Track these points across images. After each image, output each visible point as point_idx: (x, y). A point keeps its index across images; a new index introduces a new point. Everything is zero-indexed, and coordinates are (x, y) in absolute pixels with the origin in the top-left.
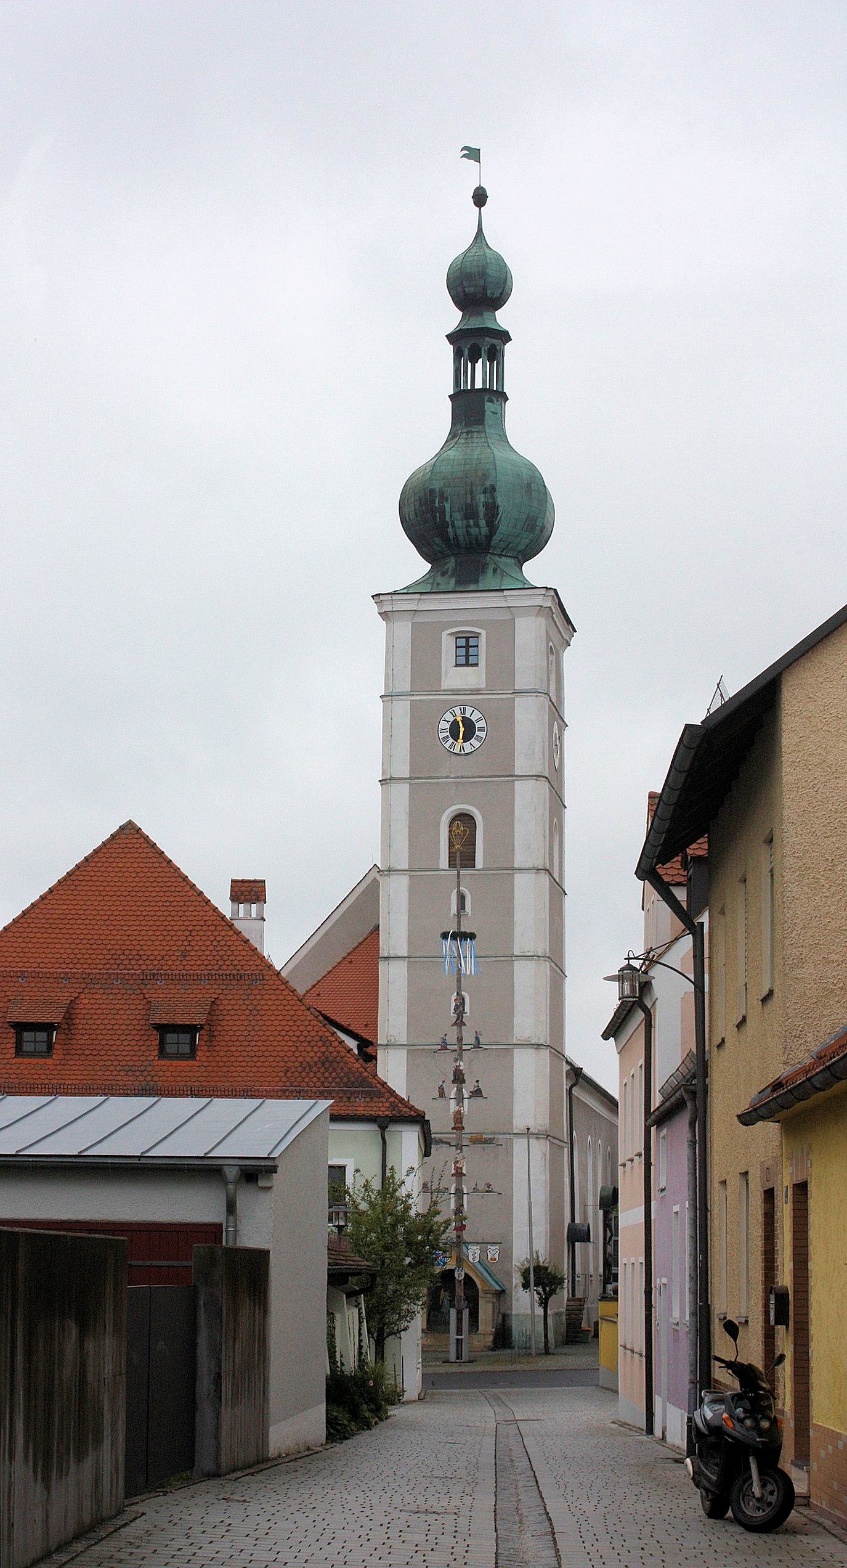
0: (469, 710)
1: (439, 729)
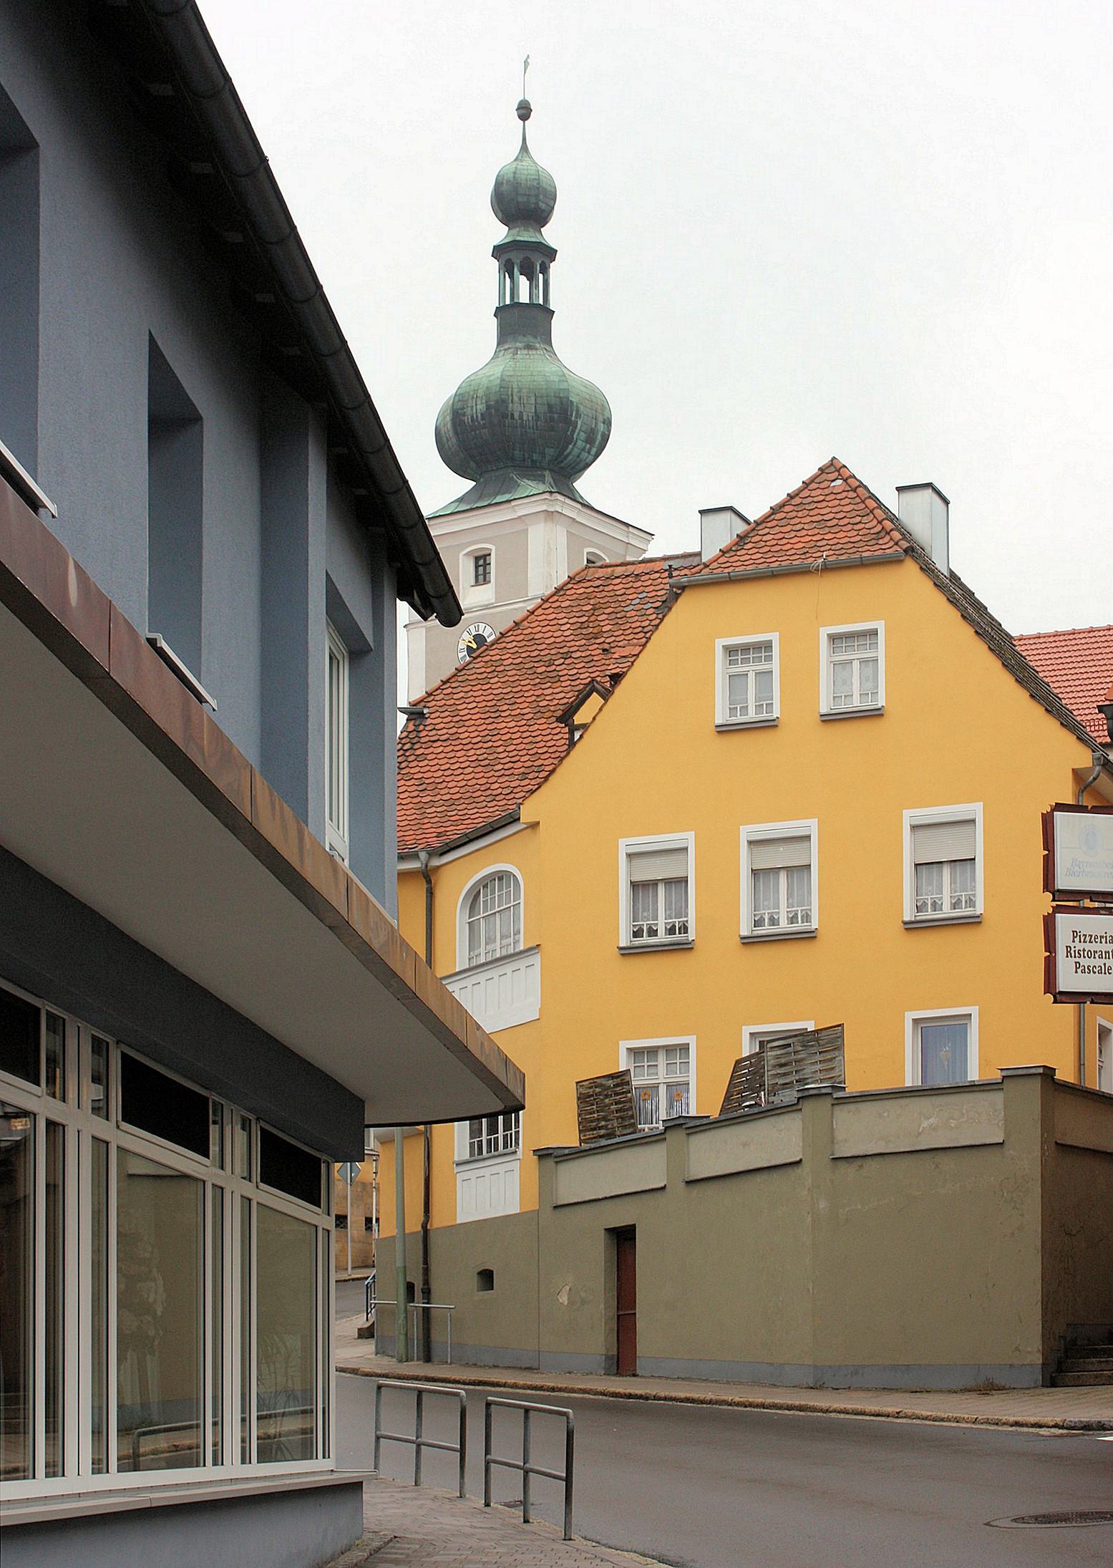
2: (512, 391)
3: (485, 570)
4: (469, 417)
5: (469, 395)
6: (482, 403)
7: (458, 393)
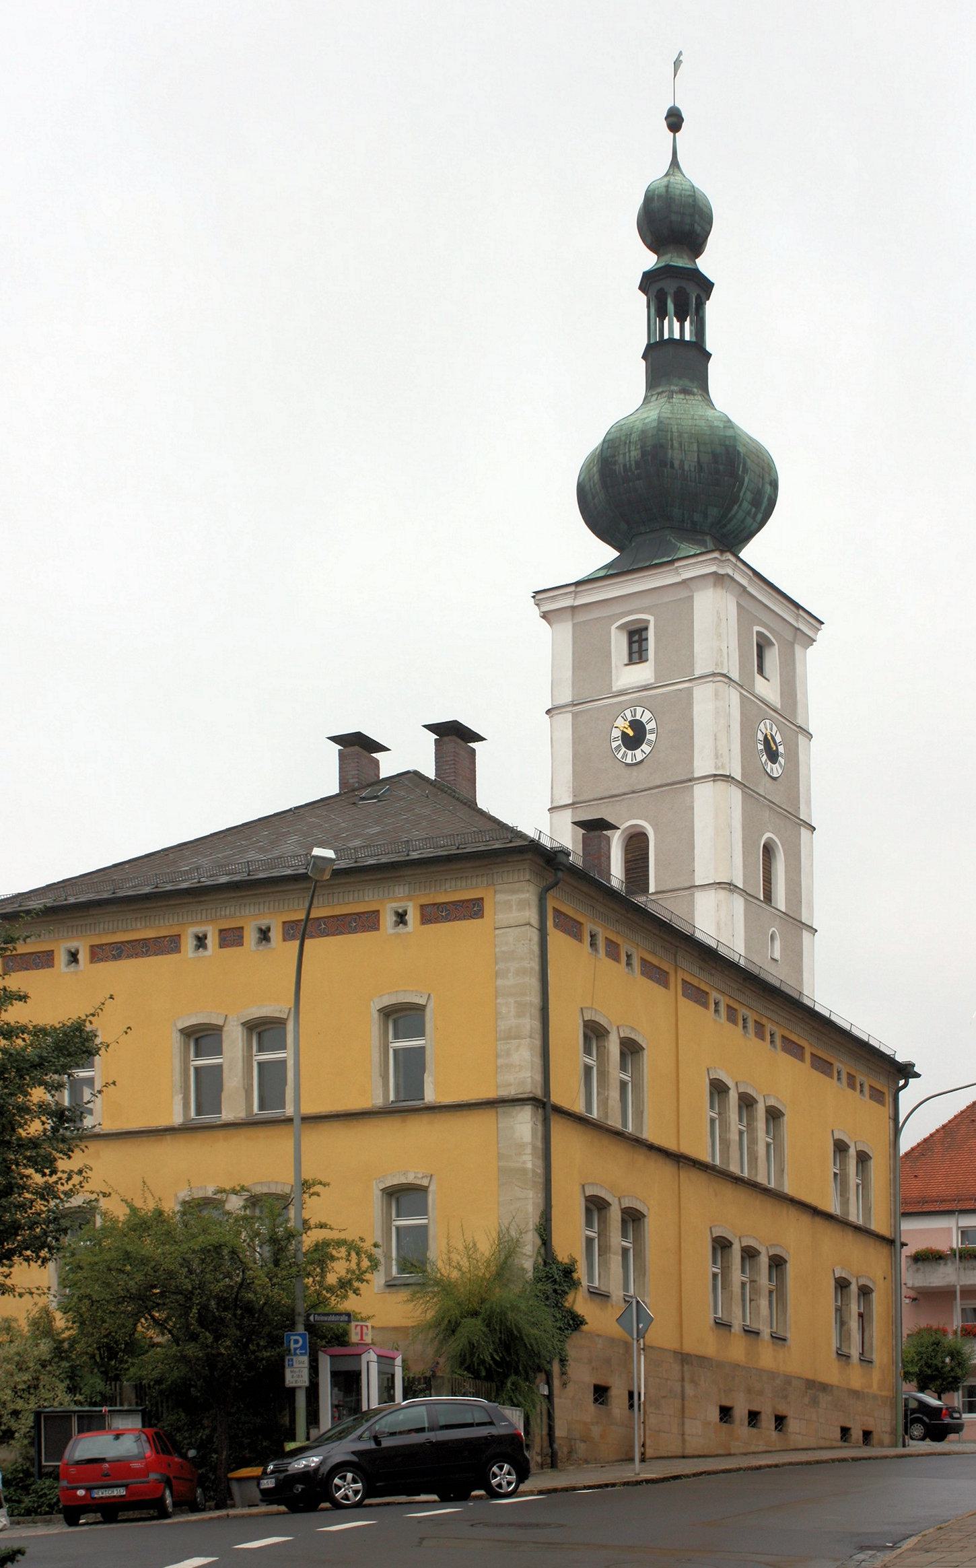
0: (639, 710)
2: (672, 435)
3: (640, 646)
4: (622, 466)
5: (620, 440)
6: (635, 450)
7: (607, 439)
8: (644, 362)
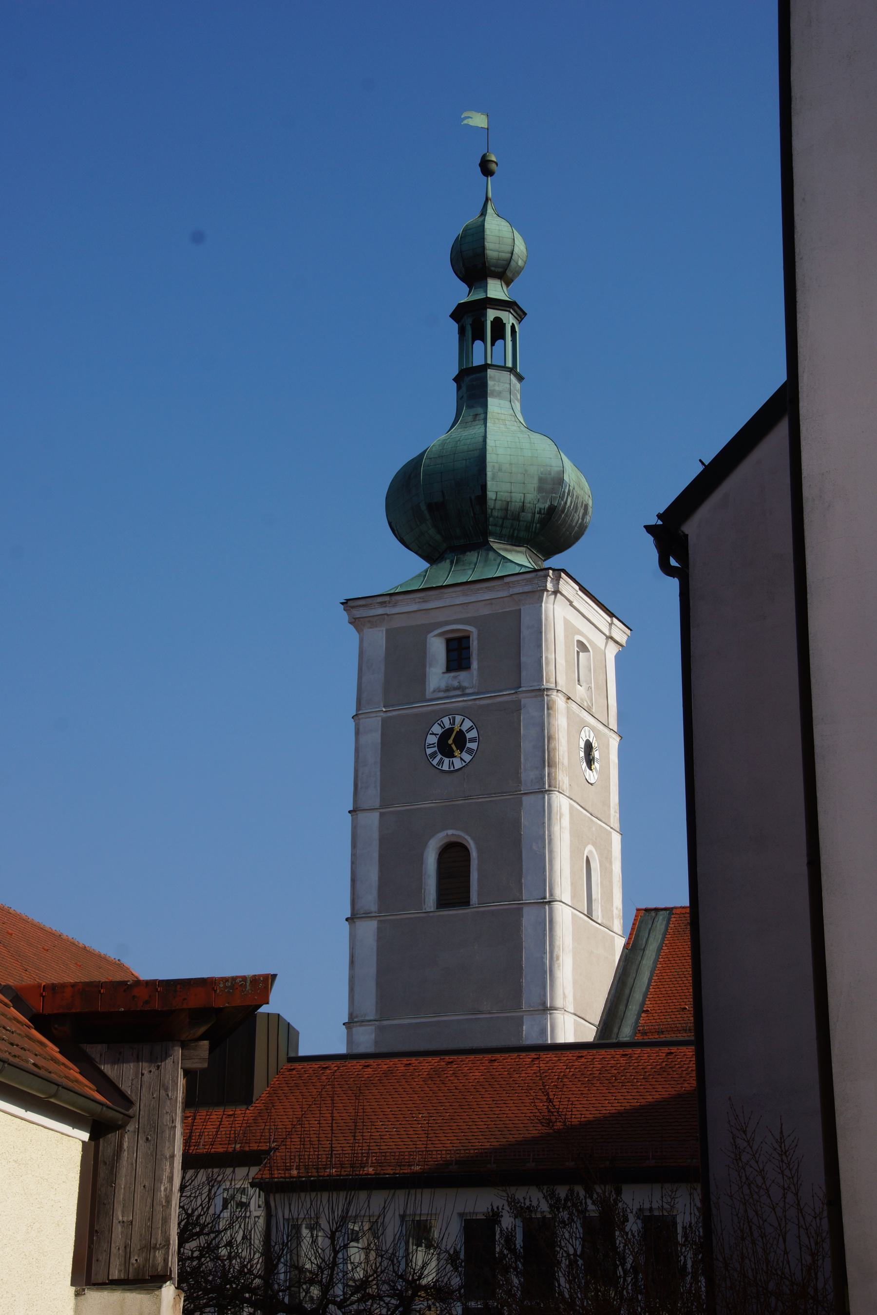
0: (459, 719)
1: (427, 744)
8: (455, 385)
